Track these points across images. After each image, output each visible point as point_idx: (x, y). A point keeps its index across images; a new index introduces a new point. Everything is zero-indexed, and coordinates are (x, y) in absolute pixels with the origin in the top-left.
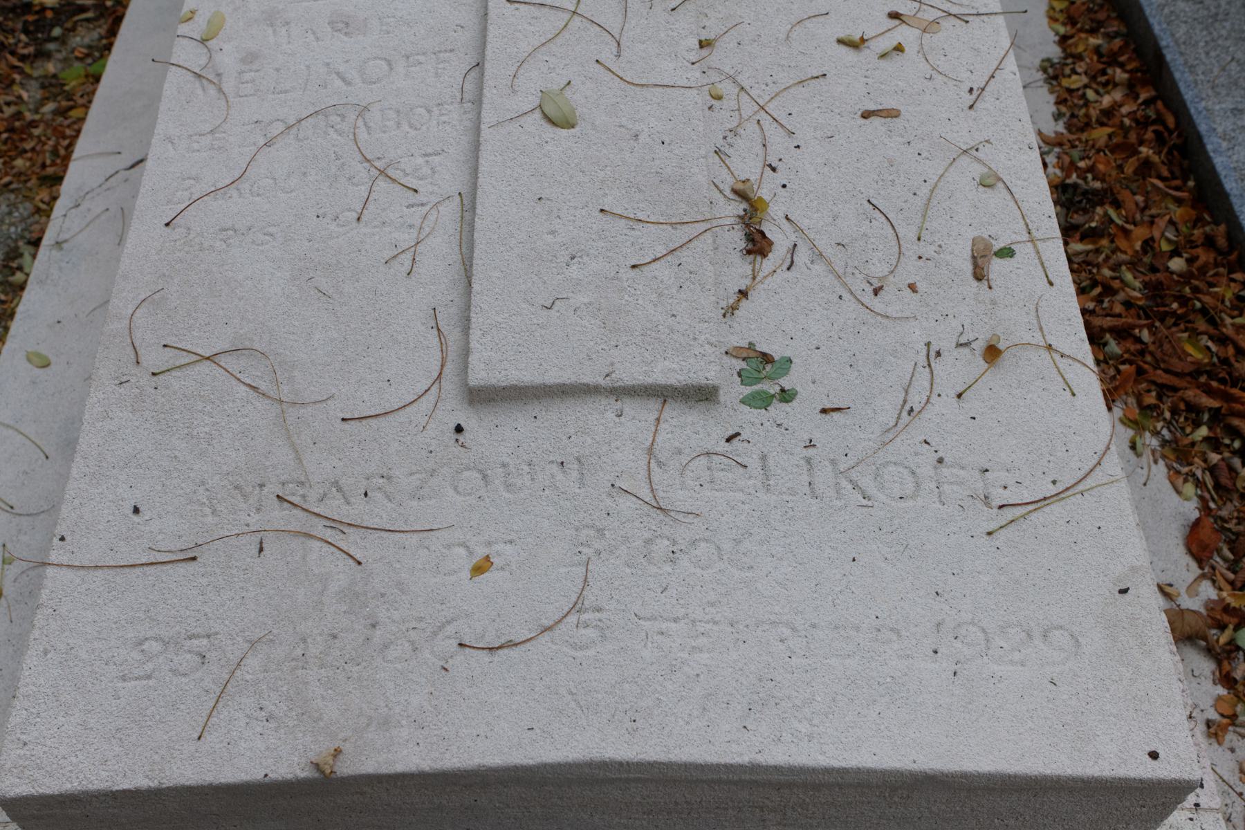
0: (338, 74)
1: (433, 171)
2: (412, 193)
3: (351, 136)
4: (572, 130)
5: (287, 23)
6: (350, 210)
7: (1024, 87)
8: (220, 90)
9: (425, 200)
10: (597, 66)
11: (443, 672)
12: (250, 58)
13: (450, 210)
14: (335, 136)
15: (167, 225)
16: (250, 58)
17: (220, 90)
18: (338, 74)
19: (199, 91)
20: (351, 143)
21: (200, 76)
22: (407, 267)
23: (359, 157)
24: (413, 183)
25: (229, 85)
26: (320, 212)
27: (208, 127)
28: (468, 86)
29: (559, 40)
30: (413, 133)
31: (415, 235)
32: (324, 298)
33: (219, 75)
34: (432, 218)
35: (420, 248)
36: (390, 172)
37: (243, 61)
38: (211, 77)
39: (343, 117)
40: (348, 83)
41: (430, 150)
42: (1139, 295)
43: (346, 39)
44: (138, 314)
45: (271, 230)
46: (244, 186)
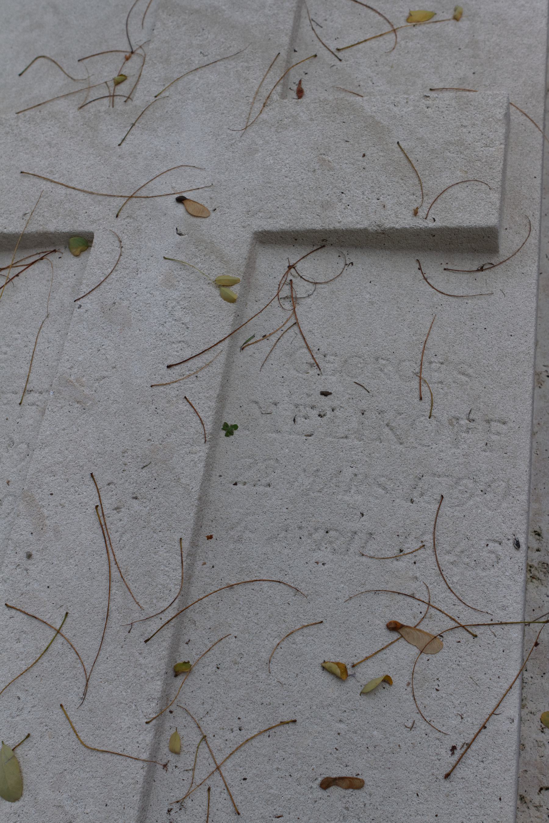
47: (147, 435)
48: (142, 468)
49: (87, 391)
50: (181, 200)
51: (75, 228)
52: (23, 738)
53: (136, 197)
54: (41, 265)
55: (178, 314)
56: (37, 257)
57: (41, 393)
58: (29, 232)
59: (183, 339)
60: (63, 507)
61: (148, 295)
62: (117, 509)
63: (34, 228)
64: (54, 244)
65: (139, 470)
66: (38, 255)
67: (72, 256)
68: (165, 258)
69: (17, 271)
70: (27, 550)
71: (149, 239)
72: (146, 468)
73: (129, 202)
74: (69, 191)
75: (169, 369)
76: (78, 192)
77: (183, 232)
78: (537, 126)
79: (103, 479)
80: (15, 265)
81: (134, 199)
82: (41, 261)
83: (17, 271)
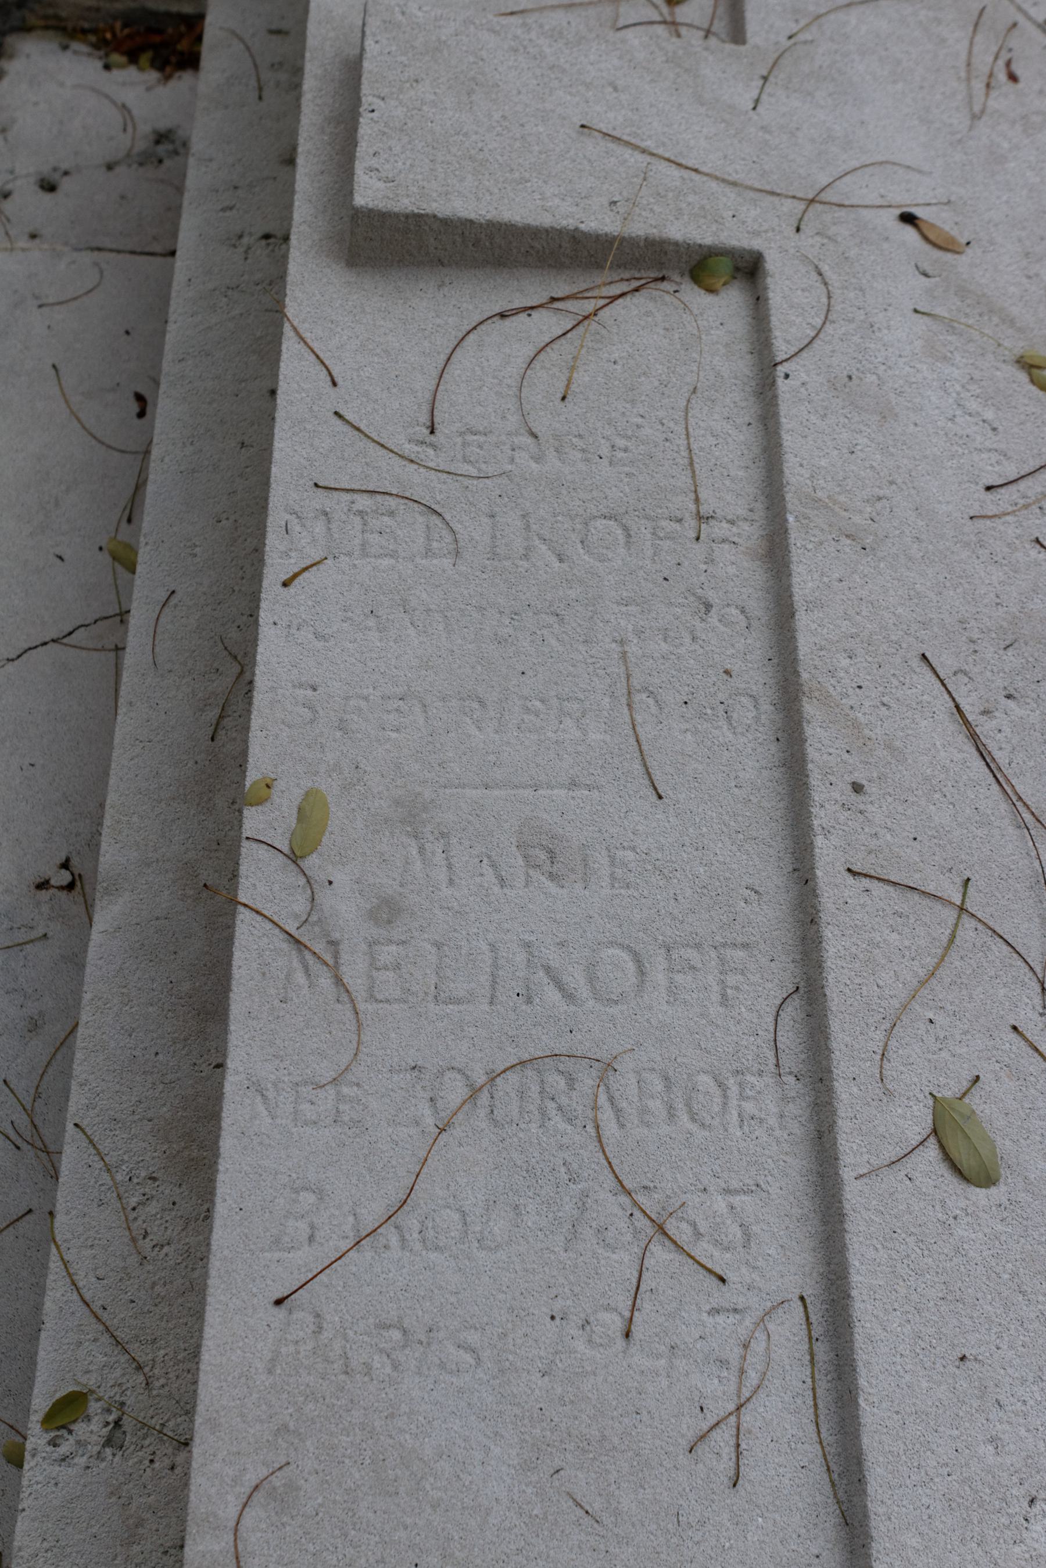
0: (548, 969)
1: (748, 1236)
2: (715, 1282)
3: (591, 1129)
4: (993, 1190)
5: (443, 835)
6: (608, 1308)
7: (173, 253)
8: (338, 981)
9: (741, 1301)
10: (1013, 1036)
11: (725, 677)
12: (386, 911)
13: (788, 1332)
14: (563, 1126)
15: (279, 1302)
16: (386, 911)
17: (338, 981)
18: (548, 969)
19: (300, 978)
20: (593, 1146)
21: (298, 942)
22: (725, 1466)
23: (610, 1182)
24: (719, 1260)
25: (354, 972)
26: (558, 1305)
27: (326, 1071)
28: (788, 1038)
29: (945, 974)
30: (701, 1134)
31: (733, 1388)
32: (587, 1520)
33: (333, 944)
34: (759, 1346)
35: (747, 1417)
36: (671, 1227)
37: (373, 916)
38: (319, 947)
39: (571, 1081)
40: (569, 997)
41: (735, 1184)
42: (755, 605)
43: (551, 887)
44: (247, 1521)
45: (473, 1338)
46: (411, 1221)
47: (992, 595)
48: (1005, 649)
49: (857, 519)
50: (908, 219)
51: (722, 238)
52: (966, 1084)
53: (821, 203)
54: (639, 299)
55: (973, 405)
56: (624, 287)
57: (732, 522)
58: (634, 235)
59: (995, 446)
60: (889, 707)
61: (907, 368)
62: (985, 712)
63: (640, 228)
64: (661, 265)
65: (1001, 652)
66: (626, 283)
67: (703, 292)
68: (916, 311)
69: (589, 306)
70: (849, 779)
71: (873, 276)
72: (1010, 649)
73: (810, 209)
74: (687, 174)
75: (988, 493)
76: (705, 178)
77: (930, 273)
78: (295, 329)
79: (946, 664)
80: (580, 295)
81: (817, 205)
82: (637, 294)
83: (589, 306)
